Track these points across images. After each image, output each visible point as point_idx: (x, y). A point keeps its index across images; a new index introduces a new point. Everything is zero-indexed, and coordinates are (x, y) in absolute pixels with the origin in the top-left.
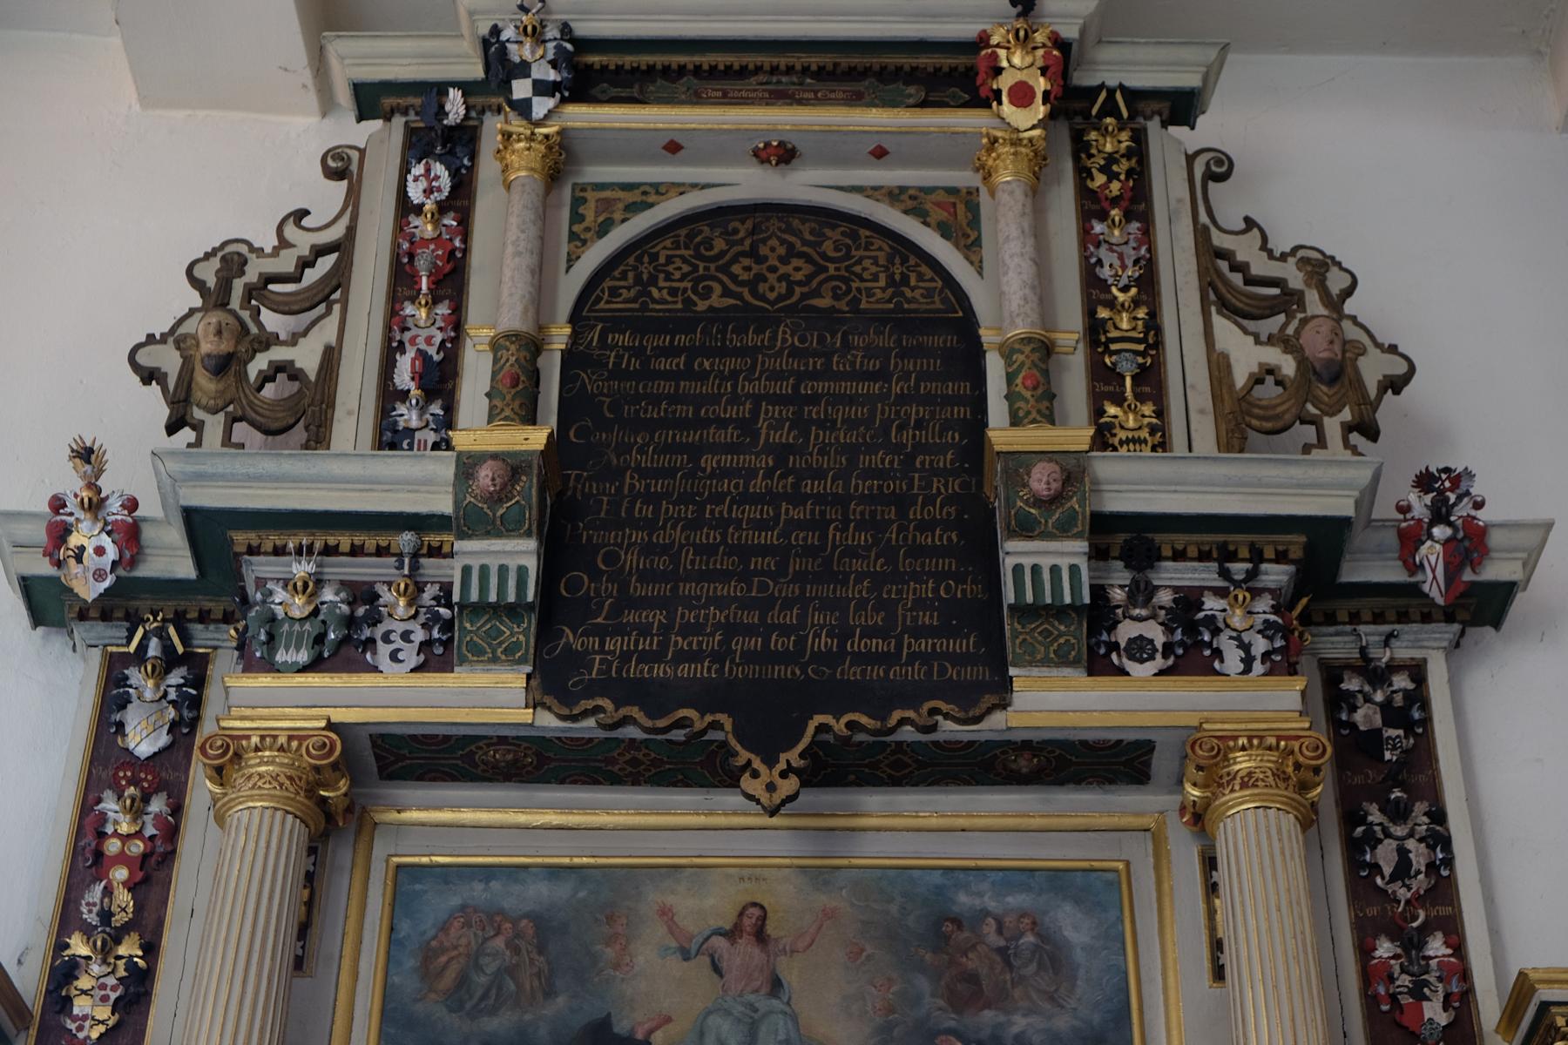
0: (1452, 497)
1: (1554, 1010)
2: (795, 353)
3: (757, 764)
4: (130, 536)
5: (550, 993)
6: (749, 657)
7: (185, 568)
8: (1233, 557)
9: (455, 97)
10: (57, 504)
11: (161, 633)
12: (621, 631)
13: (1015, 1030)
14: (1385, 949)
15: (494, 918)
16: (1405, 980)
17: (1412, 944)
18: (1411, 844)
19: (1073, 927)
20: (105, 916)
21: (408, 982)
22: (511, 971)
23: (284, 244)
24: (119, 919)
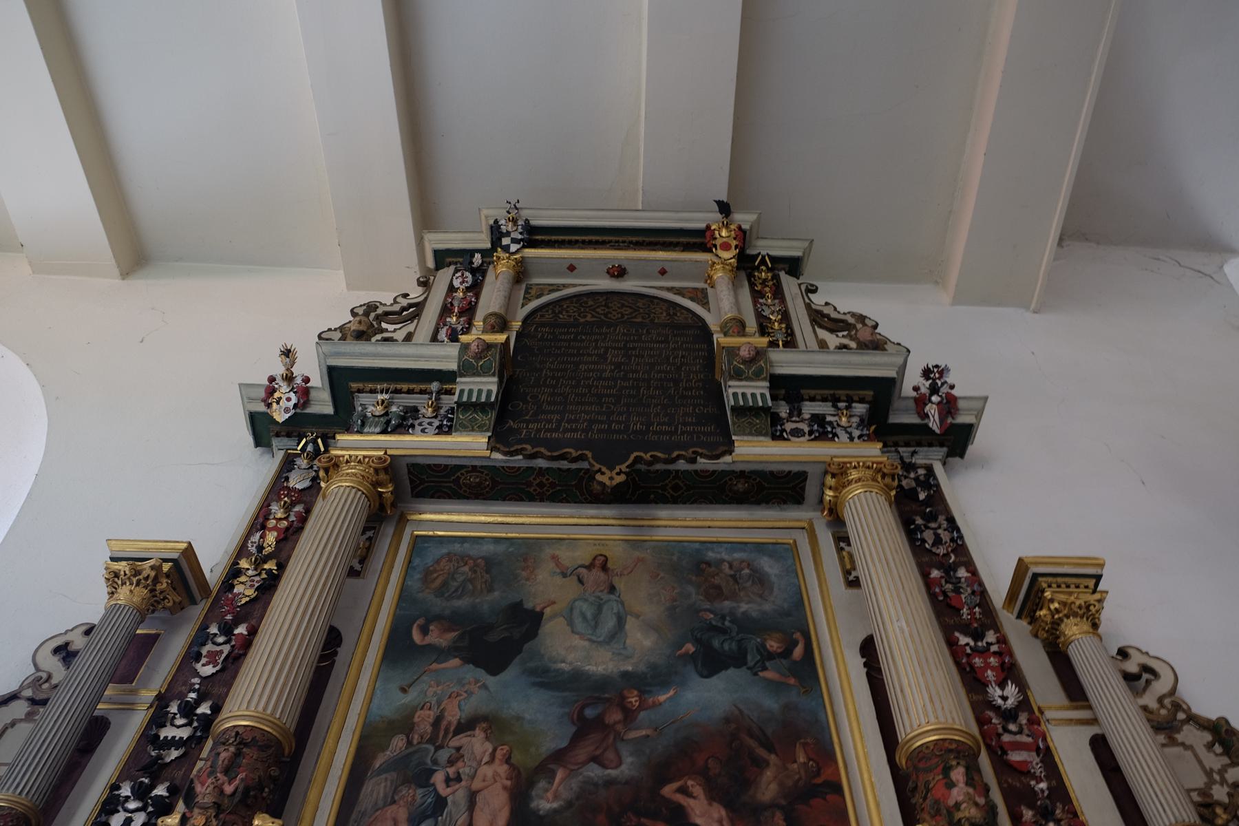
0: (939, 383)
1: (1040, 579)
2: (624, 334)
3: (604, 469)
4: (304, 393)
5: (490, 590)
6: (600, 431)
7: (329, 410)
8: (840, 401)
9: (478, 256)
10: (272, 379)
11: (315, 442)
12: (538, 421)
13: (742, 610)
14: (935, 573)
15: (464, 558)
16: (949, 586)
17: (949, 570)
18: (940, 531)
19: (769, 566)
20: (260, 548)
21: (415, 583)
22: (471, 581)
23: (395, 301)
24: (268, 550)
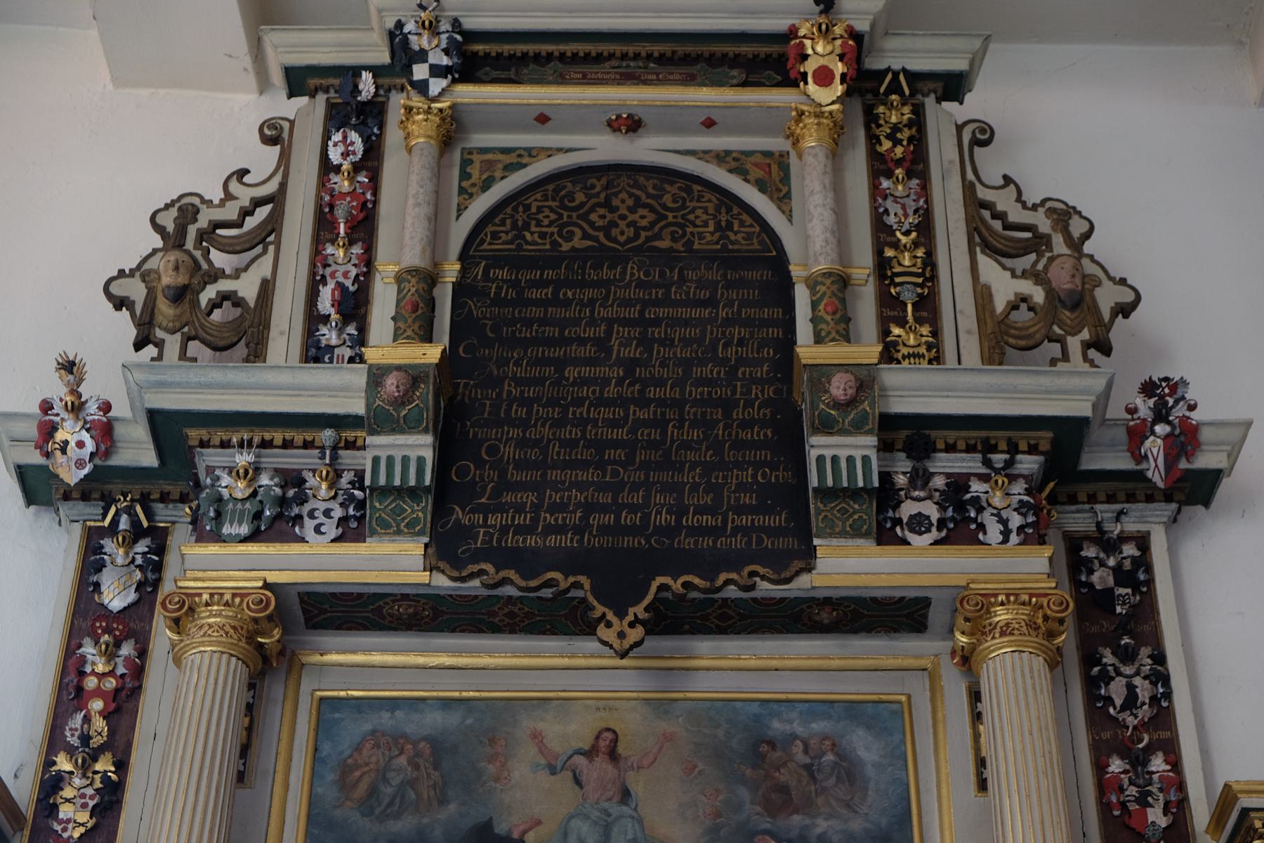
0: (1171, 401)
1: (1253, 814)
2: (640, 285)
3: (610, 616)
4: (105, 432)
5: (443, 801)
6: (604, 530)
7: (149, 458)
8: (994, 449)
9: (367, 78)
10: (46, 407)
11: (130, 511)
12: (500, 509)
13: (818, 831)
14: (1116, 765)
15: (398, 740)
16: (1133, 791)
18: (1137, 681)
19: (865, 748)
20: (85, 739)
21: (329, 792)
22: (412, 783)
23: (229, 197)
24: (96, 741)
